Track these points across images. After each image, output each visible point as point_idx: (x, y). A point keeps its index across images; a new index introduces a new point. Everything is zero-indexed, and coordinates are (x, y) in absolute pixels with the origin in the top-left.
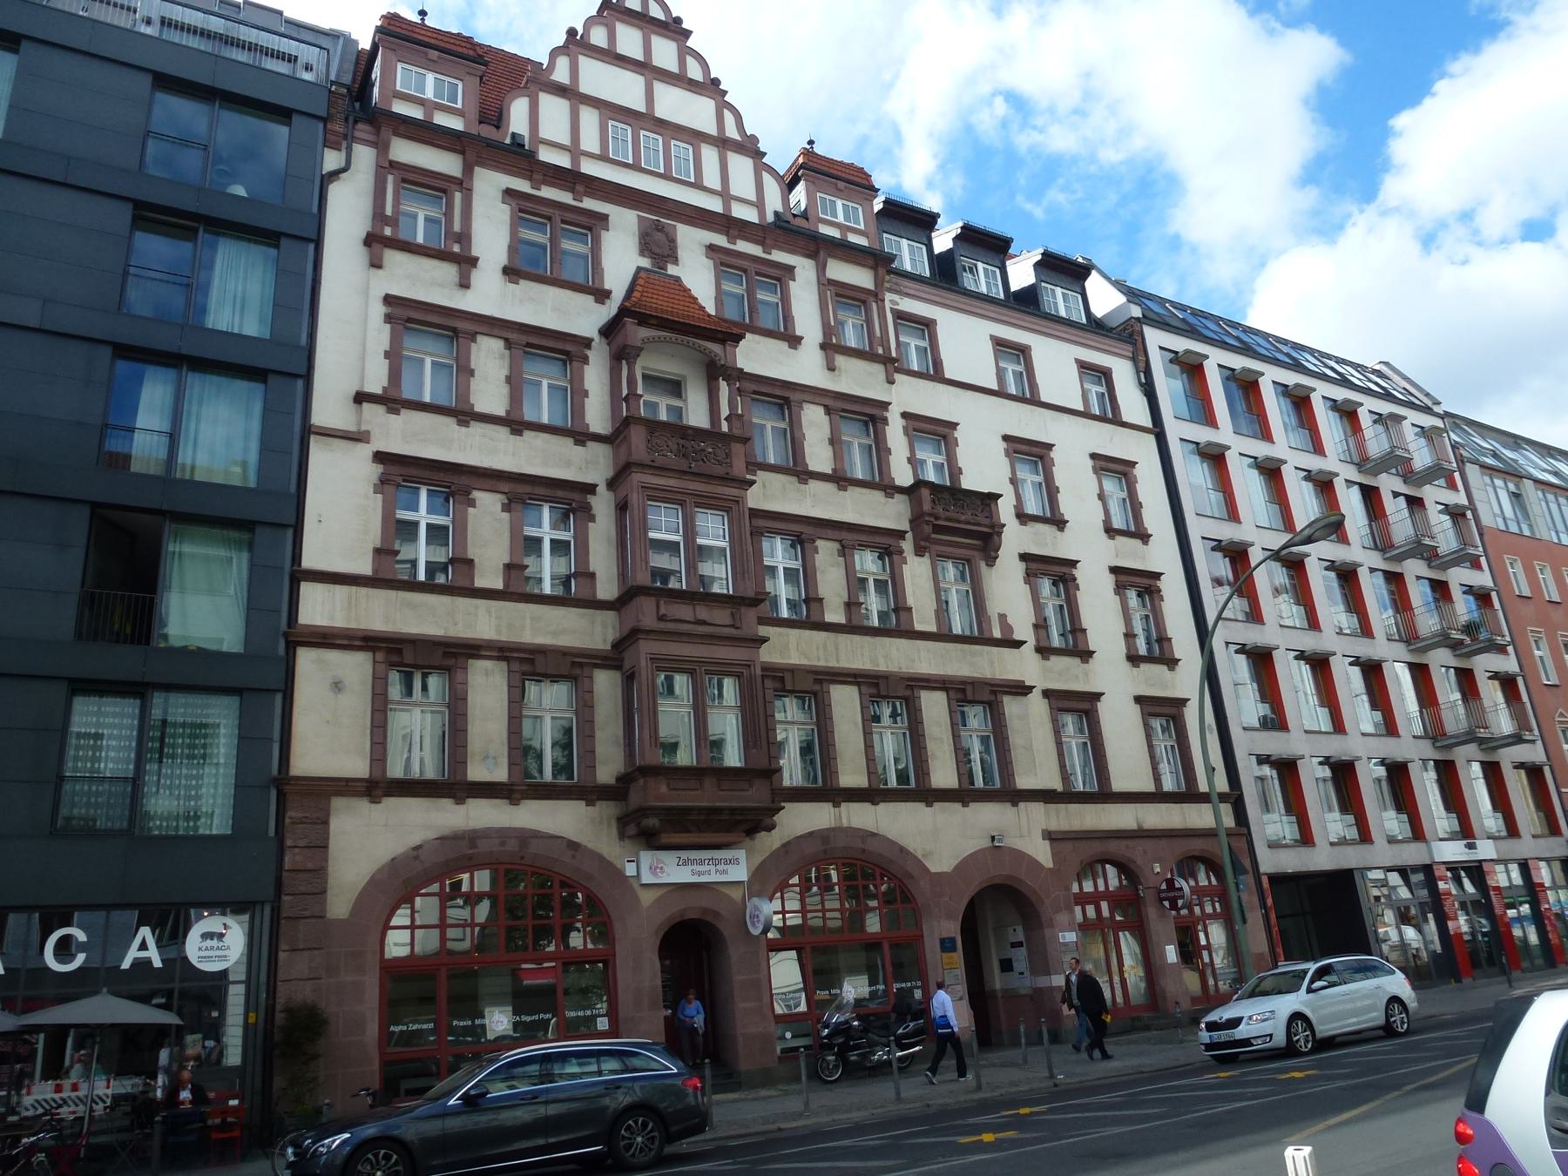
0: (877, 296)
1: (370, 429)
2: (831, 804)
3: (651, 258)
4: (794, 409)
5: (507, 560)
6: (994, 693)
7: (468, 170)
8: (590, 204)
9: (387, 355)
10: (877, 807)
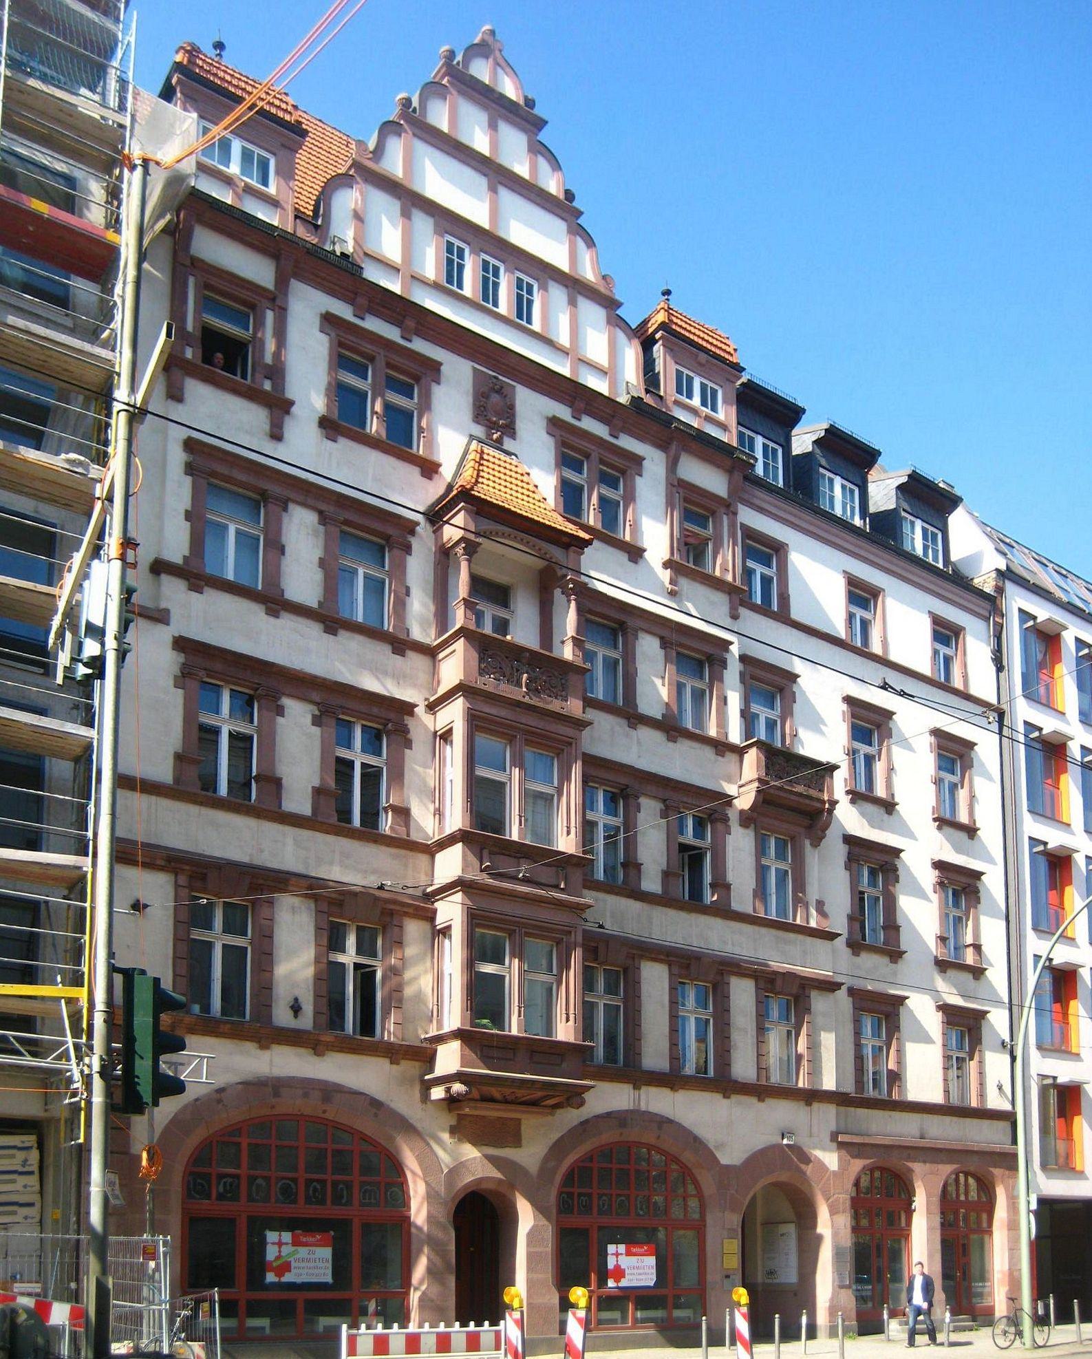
0: (728, 506)
1: (169, 607)
2: (631, 1086)
3: (486, 426)
4: (630, 637)
5: (317, 783)
6: (721, 973)
7: (282, 281)
8: (420, 346)
9: (188, 516)
10: (676, 1094)
